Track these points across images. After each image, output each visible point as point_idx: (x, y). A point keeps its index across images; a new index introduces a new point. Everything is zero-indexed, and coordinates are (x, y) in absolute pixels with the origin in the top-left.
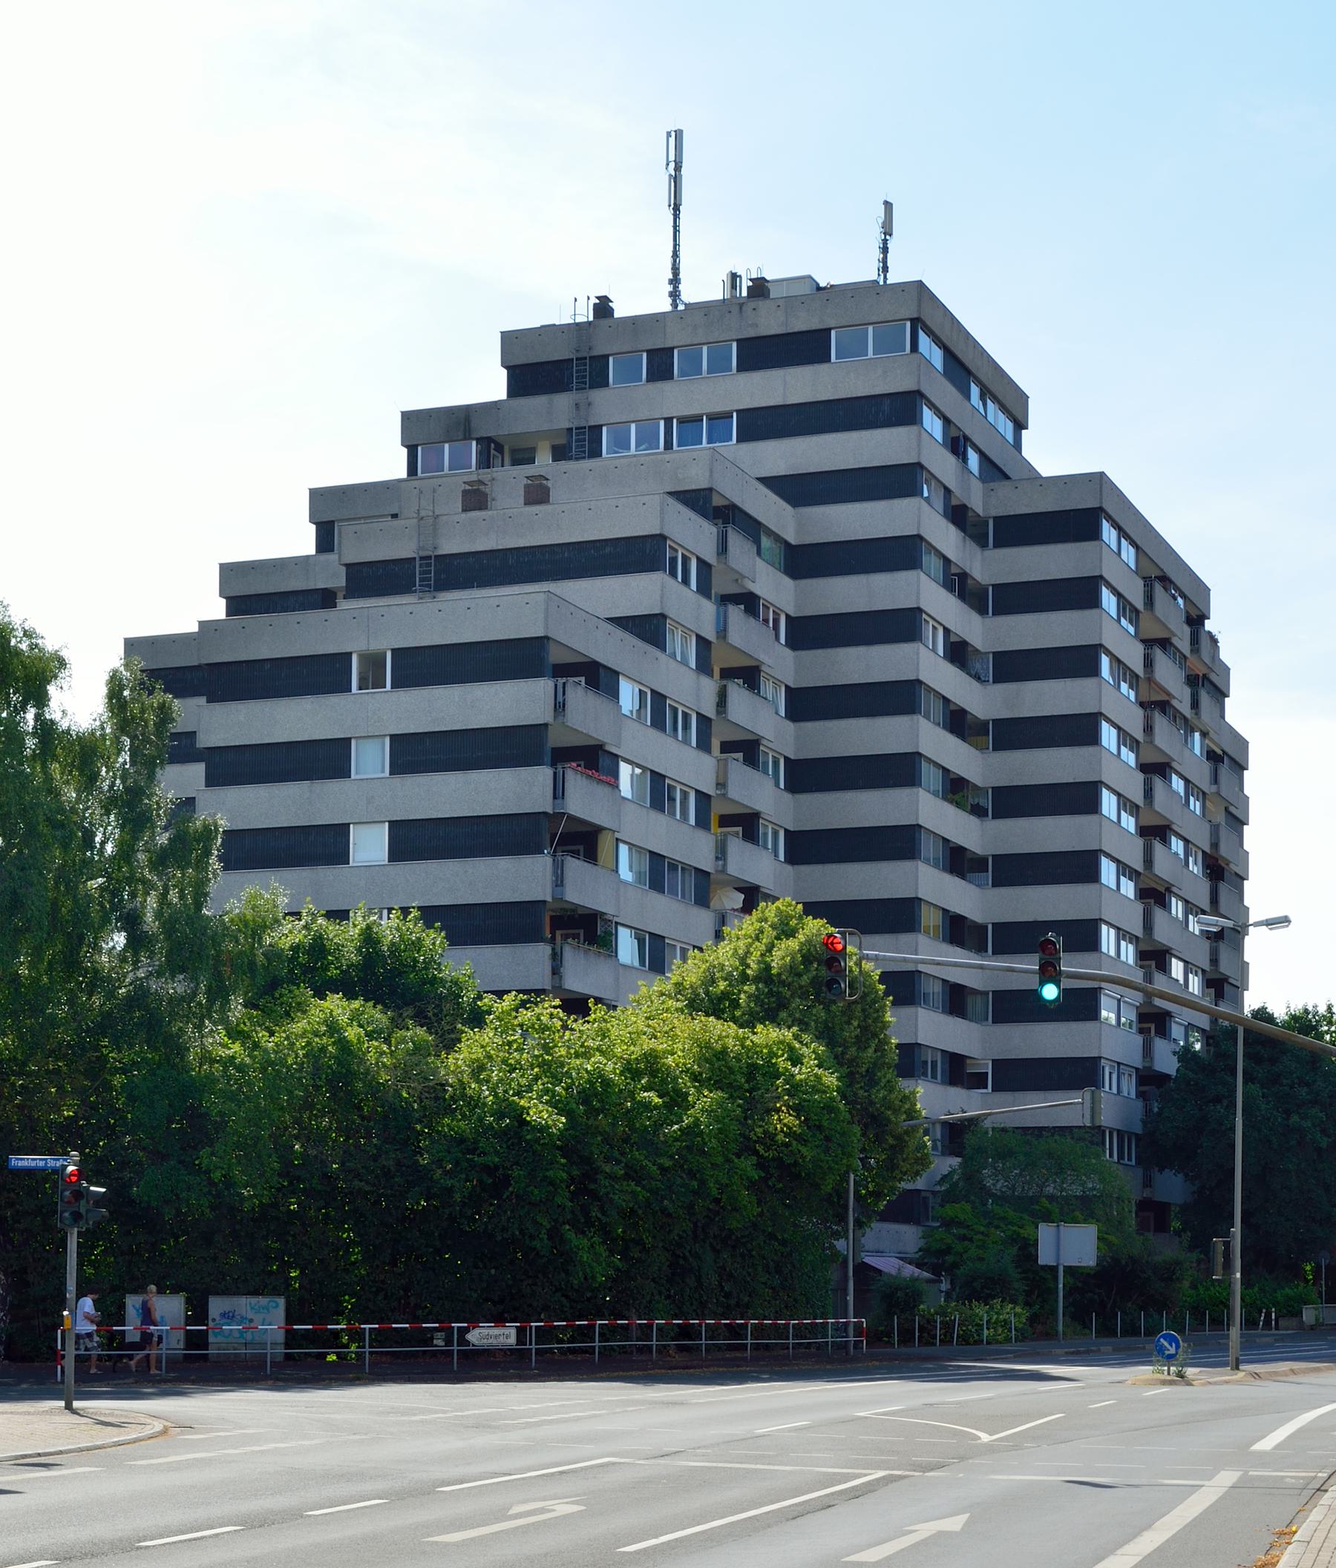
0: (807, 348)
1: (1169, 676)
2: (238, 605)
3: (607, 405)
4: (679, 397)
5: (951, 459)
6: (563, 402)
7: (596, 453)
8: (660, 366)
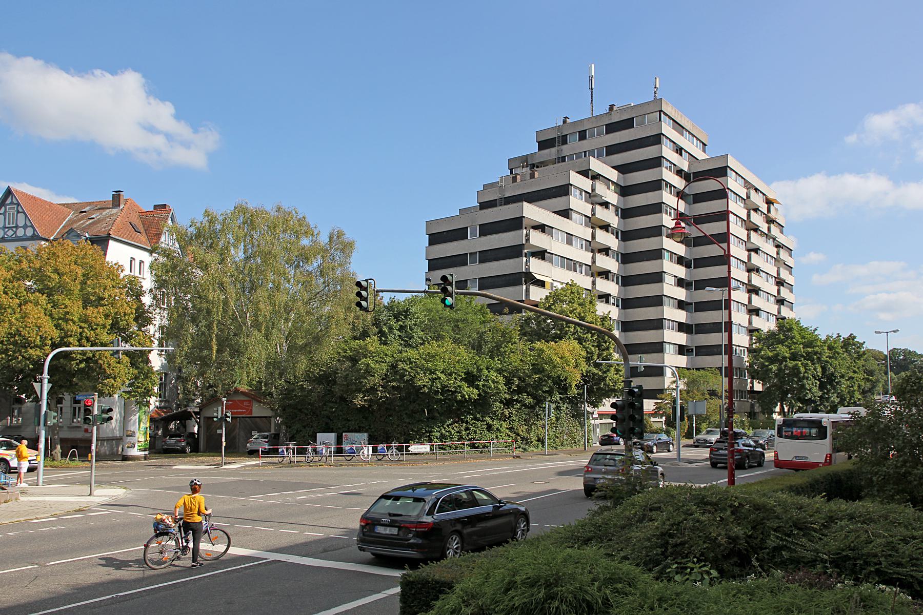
0: (628, 124)
1: (757, 219)
2: (544, 145)
3: (566, 150)
4: (586, 145)
6: (554, 150)
8: (582, 136)
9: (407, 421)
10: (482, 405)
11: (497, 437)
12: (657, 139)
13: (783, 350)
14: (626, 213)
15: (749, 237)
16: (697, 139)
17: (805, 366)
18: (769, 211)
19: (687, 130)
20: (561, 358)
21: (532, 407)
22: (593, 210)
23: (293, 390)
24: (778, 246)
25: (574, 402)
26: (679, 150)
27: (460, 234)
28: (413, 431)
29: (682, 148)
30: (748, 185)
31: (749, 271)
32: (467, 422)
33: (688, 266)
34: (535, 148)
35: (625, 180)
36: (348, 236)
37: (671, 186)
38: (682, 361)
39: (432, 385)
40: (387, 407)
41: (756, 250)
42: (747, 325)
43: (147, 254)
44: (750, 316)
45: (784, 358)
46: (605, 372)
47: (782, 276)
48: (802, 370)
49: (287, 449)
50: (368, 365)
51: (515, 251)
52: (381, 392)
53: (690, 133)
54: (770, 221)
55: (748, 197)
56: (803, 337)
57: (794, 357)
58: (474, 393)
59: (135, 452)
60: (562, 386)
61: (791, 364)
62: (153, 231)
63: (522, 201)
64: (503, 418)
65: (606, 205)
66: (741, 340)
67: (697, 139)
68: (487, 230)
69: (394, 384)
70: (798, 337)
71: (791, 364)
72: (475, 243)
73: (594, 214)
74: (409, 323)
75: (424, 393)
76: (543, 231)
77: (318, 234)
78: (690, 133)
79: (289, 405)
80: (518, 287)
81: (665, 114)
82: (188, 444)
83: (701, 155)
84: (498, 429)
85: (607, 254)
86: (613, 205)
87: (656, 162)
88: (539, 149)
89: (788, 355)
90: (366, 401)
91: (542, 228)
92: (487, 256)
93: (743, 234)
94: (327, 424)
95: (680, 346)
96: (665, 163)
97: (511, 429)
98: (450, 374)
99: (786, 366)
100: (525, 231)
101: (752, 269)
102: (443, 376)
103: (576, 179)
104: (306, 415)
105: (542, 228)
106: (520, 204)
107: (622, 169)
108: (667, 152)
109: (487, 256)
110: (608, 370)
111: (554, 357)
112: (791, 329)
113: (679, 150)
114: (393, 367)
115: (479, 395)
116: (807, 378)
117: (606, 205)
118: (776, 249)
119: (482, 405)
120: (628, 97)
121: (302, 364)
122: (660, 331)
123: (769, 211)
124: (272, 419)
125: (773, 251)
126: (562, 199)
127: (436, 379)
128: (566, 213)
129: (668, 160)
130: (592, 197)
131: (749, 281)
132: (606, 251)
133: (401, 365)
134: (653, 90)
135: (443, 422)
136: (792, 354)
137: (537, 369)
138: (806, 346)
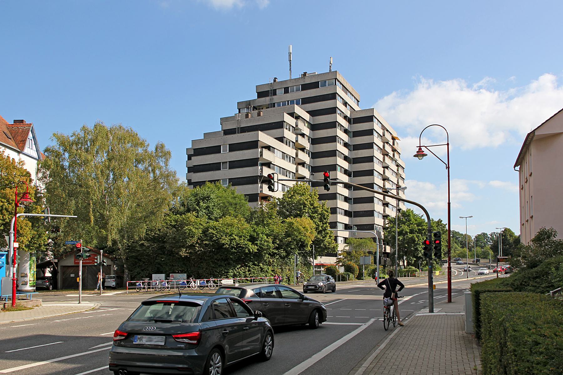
0: (315, 85)
1: (388, 149)
2: (261, 95)
3: (276, 99)
4: (289, 97)
5: (344, 107)
6: (268, 98)
7: (274, 106)
8: (286, 91)
9: (213, 266)
10: (258, 256)
11: (266, 276)
12: (333, 96)
13: (406, 228)
14: (314, 141)
15: (384, 159)
16: (355, 98)
17: (418, 237)
18: (394, 144)
19: (349, 92)
20: (304, 228)
21: (283, 258)
22: (297, 138)
23: (135, 247)
24: (397, 166)
25: (305, 256)
26: (345, 104)
27: (216, 150)
28: (216, 271)
29: (347, 104)
30: (383, 128)
31: (384, 180)
32: (249, 267)
33: (349, 175)
34: (255, 96)
35: (313, 121)
36: (167, 148)
37: (341, 126)
38: (346, 234)
39: (231, 243)
40: (201, 257)
41: (387, 167)
42: (382, 212)
43: (16, 154)
44: (384, 207)
45: (406, 233)
46: (323, 237)
47: (400, 184)
48: (417, 239)
49: (143, 283)
50: (190, 230)
51: (253, 162)
52: (198, 247)
53: (351, 94)
54: (394, 150)
55: (384, 135)
56: (416, 220)
57: (412, 232)
58: (254, 248)
59: (28, 288)
60: (302, 245)
61: (410, 236)
62: (19, 138)
63: (258, 130)
64: (269, 264)
65: (303, 135)
66: (379, 221)
67: (355, 98)
68: (233, 148)
69: (207, 242)
70: (413, 220)
71: (410, 236)
72: (226, 156)
73: (297, 141)
74: (211, 205)
75: (226, 248)
76: (269, 150)
77: (148, 145)
78: (351, 94)
79: (132, 257)
80: (255, 185)
81: (339, 81)
82: (51, 284)
83: (357, 108)
84: (266, 271)
85: (304, 166)
86: (307, 136)
87: (333, 110)
88: (258, 97)
89: (408, 231)
90: (187, 253)
91: (268, 148)
92: (233, 165)
93: (381, 157)
94: (158, 268)
95: (346, 225)
96: (338, 112)
97: (273, 271)
98: (241, 237)
99: (407, 237)
100: (259, 150)
101: (385, 179)
102: (237, 238)
103: (288, 119)
104: (144, 262)
105: (268, 148)
106: (256, 132)
107: (312, 113)
108: (340, 105)
109: (233, 165)
110: (326, 236)
111: (300, 227)
112: (409, 215)
113: (345, 104)
114: (205, 231)
115: (258, 249)
116: (419, 244)
117: (303, 135)
118: (396, 167)
119: (258, 256)
120: (317, 68)
121: (143, 230)
122: (335, 215)
123: (394, 144)
124: (112, 267)
125: (395, 168)
126: (279, 130)
127: (233, 239)
128: (281, 139)
129: (339, 110)
130: (296, 130)
131: (384, 186)
132: (303, 164)
133: (211, 231)
134: (329, 65)
135: (235, 267)
136: (410, 230)
137: (288, 235)
138: (418, 225)
